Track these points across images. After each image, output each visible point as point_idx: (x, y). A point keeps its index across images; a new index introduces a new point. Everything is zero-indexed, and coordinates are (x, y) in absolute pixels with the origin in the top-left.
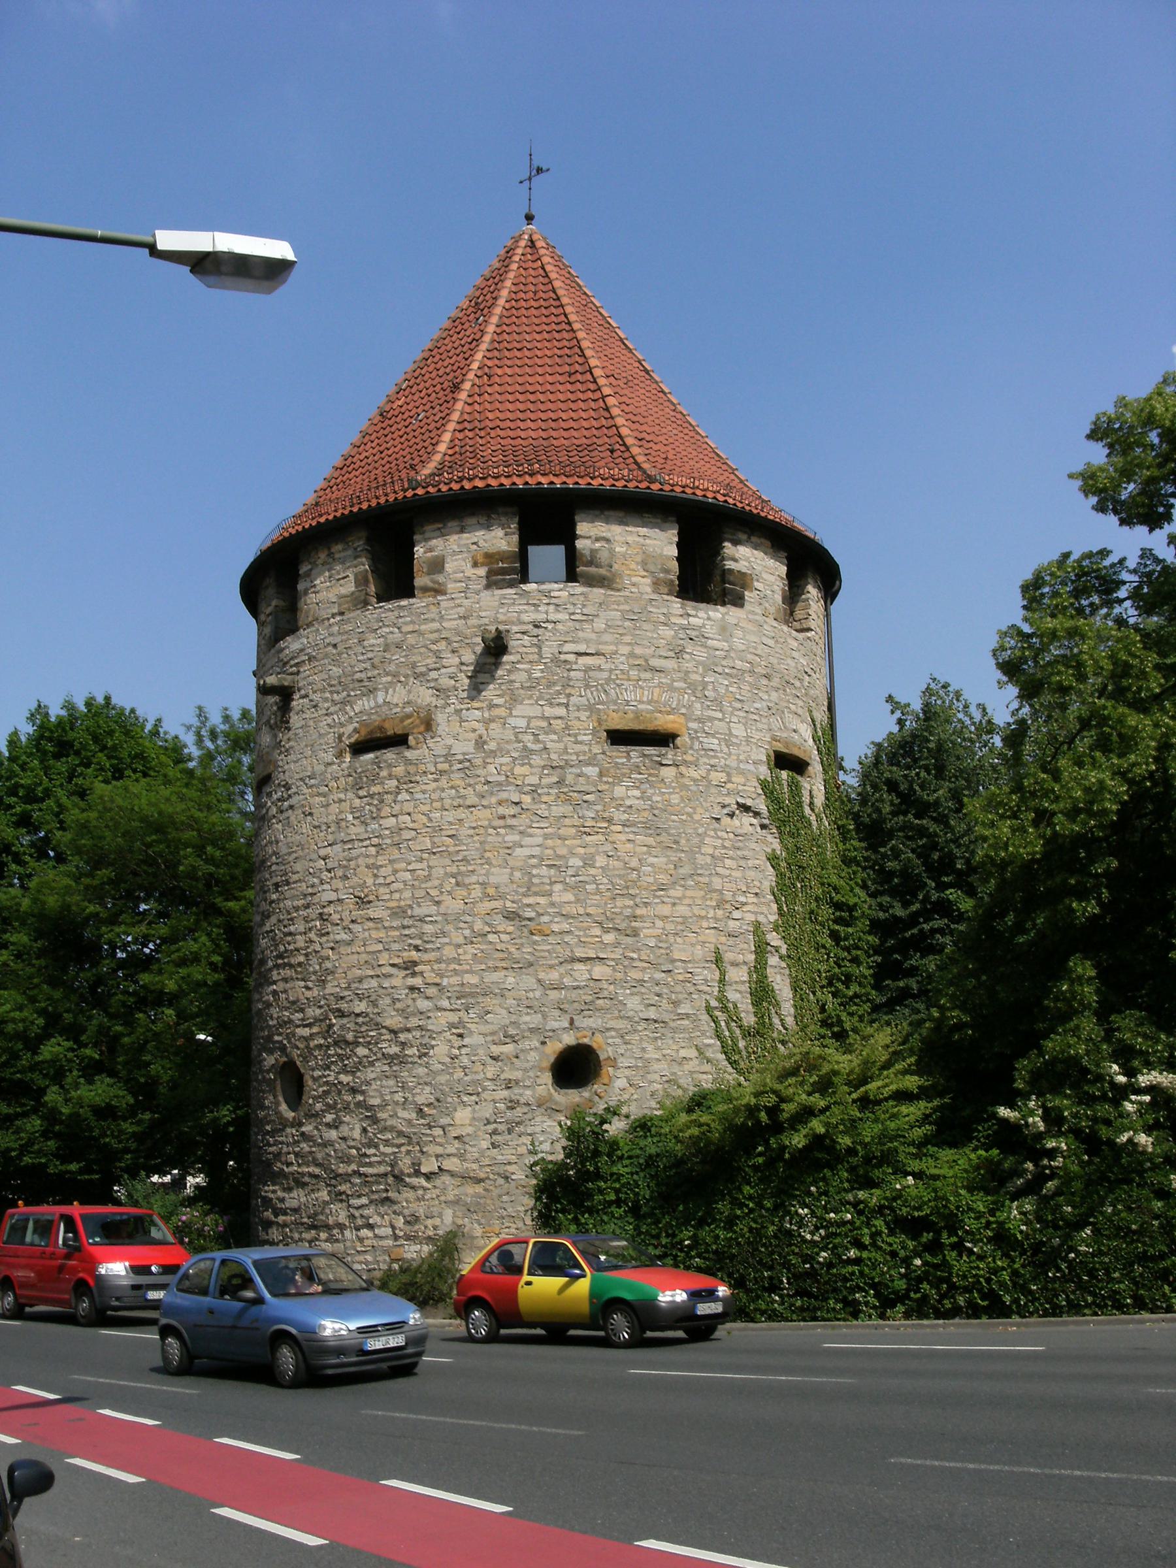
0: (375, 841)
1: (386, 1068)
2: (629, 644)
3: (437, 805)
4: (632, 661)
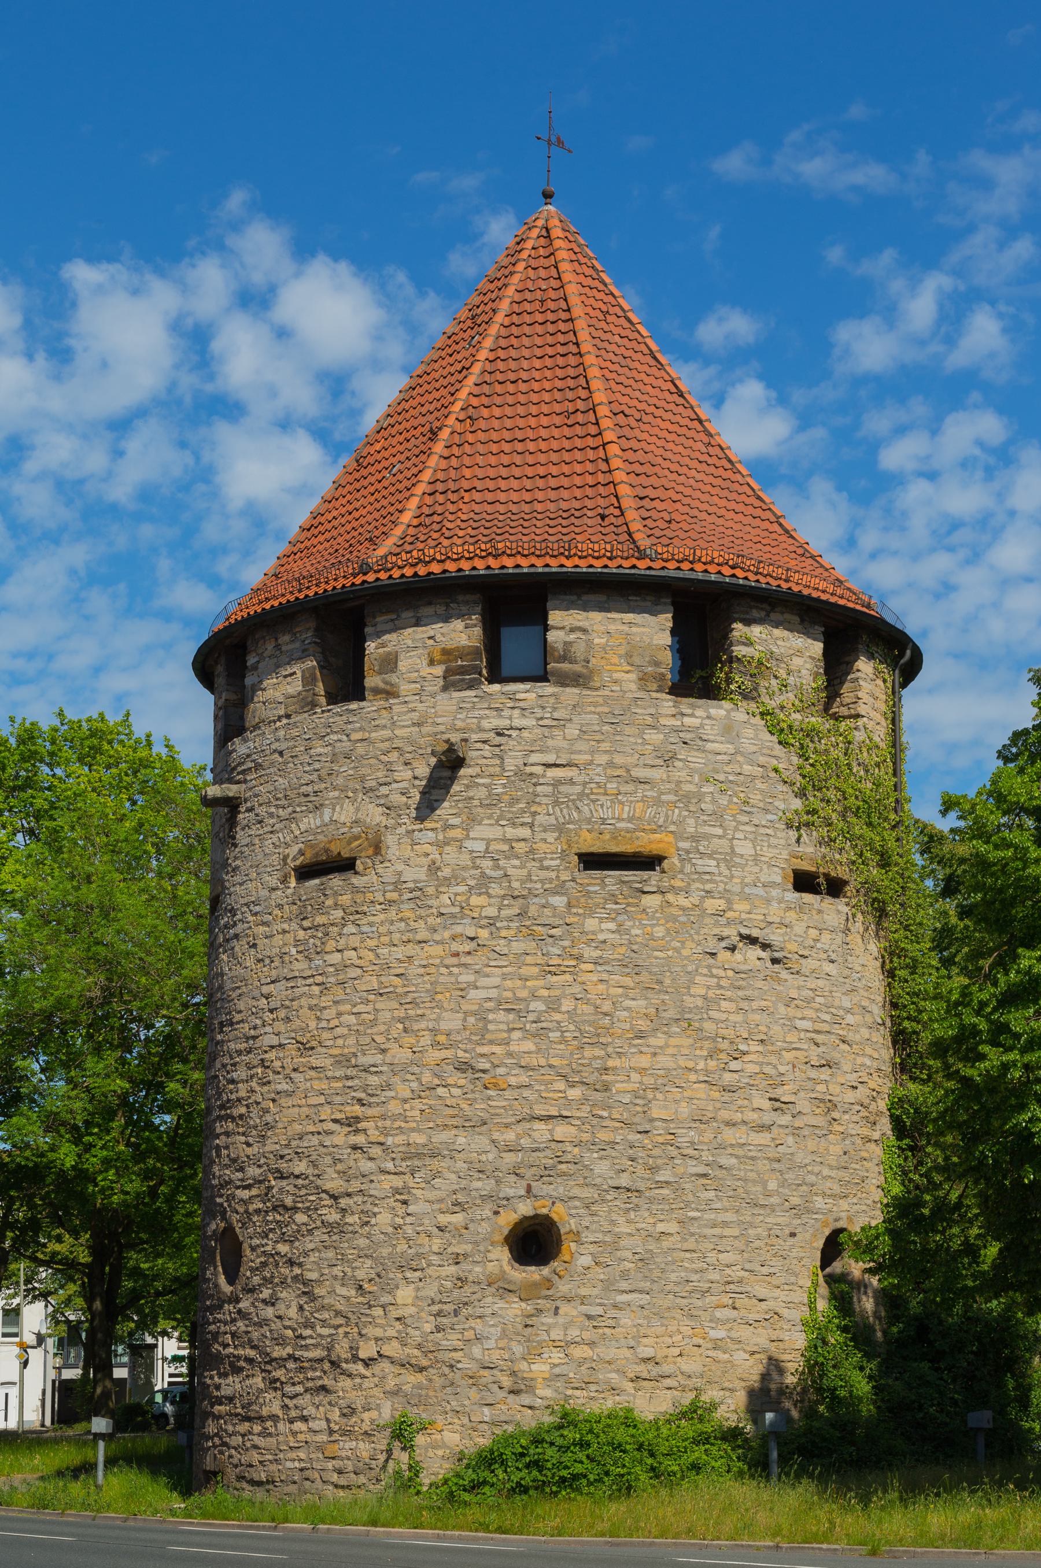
0: (319, 979)
1: (326, 1237)
2: (606, 752)
3: (385, 939)
4: (609, 771)
